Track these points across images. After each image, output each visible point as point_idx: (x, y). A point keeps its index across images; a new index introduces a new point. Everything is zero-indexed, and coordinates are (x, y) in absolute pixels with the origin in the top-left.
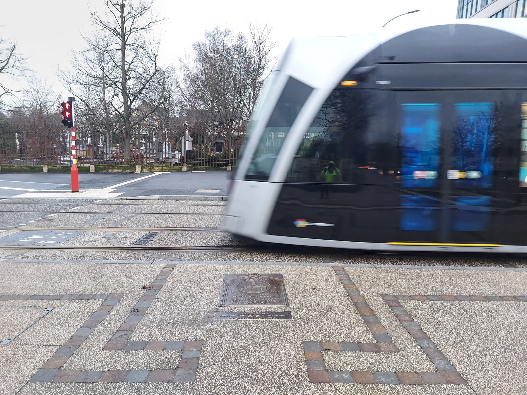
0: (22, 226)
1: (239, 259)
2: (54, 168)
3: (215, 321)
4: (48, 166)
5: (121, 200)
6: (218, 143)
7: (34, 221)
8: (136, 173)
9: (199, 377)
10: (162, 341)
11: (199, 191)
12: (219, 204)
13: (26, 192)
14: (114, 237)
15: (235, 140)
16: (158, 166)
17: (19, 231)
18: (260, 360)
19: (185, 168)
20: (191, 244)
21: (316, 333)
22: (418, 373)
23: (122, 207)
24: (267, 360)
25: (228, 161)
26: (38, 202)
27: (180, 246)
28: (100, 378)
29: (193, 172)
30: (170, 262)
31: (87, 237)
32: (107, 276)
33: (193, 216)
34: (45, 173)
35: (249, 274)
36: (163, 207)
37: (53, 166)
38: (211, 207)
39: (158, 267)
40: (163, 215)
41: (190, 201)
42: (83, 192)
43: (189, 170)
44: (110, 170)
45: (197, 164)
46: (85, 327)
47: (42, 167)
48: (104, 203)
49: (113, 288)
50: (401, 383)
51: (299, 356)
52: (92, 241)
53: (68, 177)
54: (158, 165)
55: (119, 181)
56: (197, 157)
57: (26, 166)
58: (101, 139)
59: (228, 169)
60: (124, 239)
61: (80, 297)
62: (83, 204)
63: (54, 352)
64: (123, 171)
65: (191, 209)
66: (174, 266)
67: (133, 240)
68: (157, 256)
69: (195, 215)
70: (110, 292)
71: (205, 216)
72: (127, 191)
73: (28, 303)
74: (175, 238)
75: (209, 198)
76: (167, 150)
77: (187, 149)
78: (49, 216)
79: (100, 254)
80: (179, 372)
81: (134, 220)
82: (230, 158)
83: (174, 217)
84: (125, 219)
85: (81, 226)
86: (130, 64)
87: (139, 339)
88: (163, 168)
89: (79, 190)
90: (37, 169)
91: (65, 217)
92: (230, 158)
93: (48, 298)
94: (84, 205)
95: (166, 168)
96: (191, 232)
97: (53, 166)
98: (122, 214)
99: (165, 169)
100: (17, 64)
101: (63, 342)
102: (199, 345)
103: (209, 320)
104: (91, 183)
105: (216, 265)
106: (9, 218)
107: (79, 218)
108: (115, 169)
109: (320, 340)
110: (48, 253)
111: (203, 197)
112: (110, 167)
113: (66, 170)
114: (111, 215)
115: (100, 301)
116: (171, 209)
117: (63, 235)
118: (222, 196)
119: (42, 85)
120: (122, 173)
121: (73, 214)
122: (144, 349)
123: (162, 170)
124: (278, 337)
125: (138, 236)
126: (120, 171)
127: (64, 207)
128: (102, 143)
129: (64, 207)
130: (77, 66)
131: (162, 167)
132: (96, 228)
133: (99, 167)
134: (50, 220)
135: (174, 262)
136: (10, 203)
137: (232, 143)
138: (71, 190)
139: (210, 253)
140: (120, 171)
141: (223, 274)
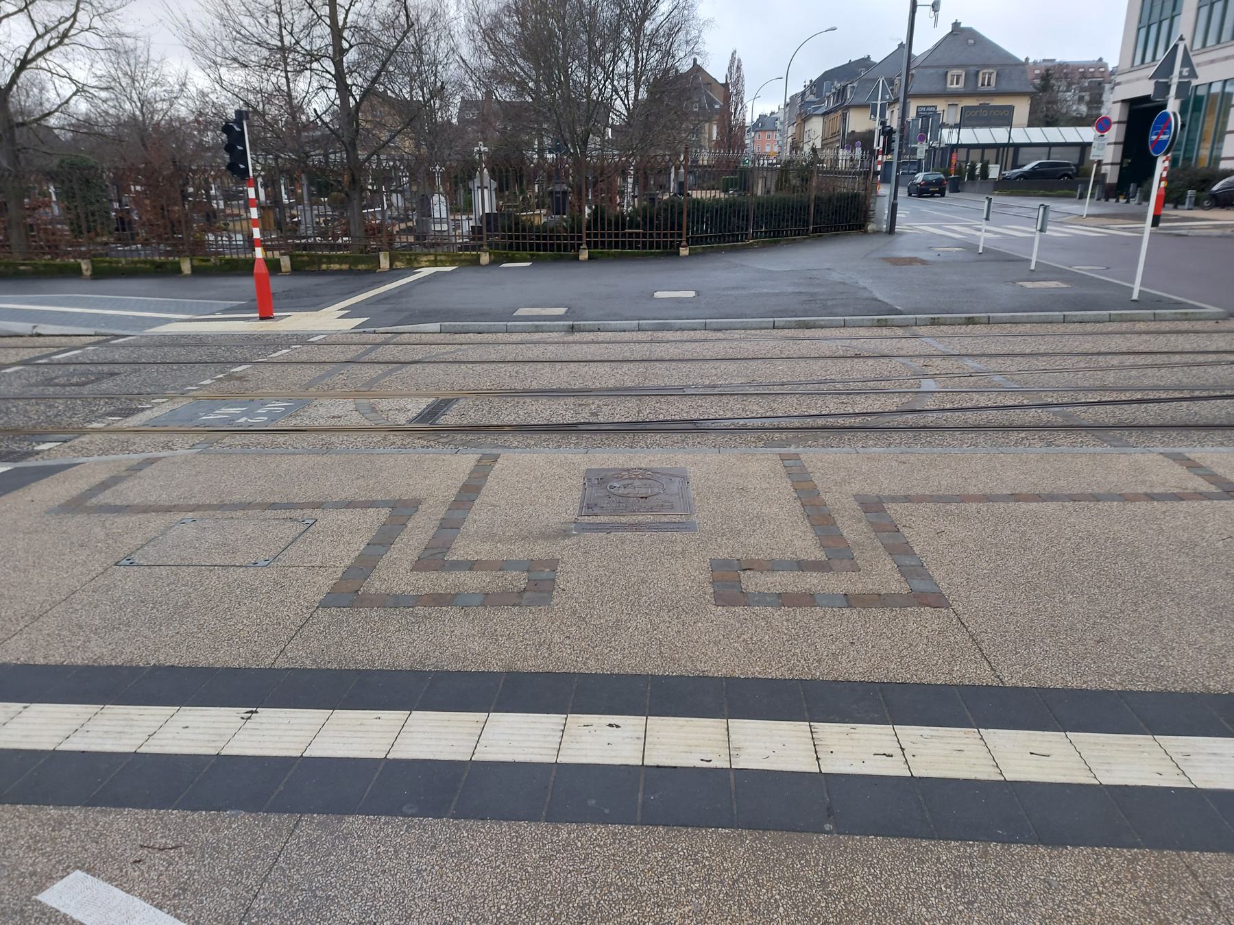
0: (193, 390)
1: (609, 445)
2: (203, 264)
3: (574, 535)
4: (191, 260)
5: (364, 335)
6: (557, 193)
7: (211, 382)
8: (380, 272)
9: (555, 601)
10: (496, 561)
11: (522, 312)
12: (566, 339)
13: (169, 321)
14: (374, 410)
15: (595, 184)
16: (426, 255)
17: (191, 400)
18: (644, 582)
19: (485, 258)
20: (519, 421)
21: (733, 549)
22: (880, 595)
23: (371, 351)
24: (655, 581)
25: (580, 238)
26: (199, 341)
27: (500, 424)
28: (417, 602)
29: (504, 265)
30: (488, 451)
31: (322, 411)
32: (385, 474)
33: (516, 367)
34: (186, 276)
35: (628, 470)
36: (453, 348)
37: (203, 260)
38: (551, 348)
39: (466, 461)
40: (457, 366)
41: (505, 334)
42: (282, 318)
43: (495, 262)
44: (324, 267)
45: (511, 247)
46: (374, 544)
47: (178, 263)
48: (331, 341)
49: (402, 489)
50: (849, 606)
51: (704, 576)
52: (334, 417)
53: (247, 285)
54: (425, 250)
55: (350, 293)
56: (510, 230)
57: (145, 262)
58: (283, 187)
59: (581, 257)
60: (394, 412)
61: (350, 505)
62: (291, 345)
63: (340, 575)
64: (353, 267)
65: (510, 352)
66: (496, 458)
67: (409, 413)
68: (461, 442)
69: (520, 364)
70: (398, 497)
71: (540, 366)
72: (376, 312)
73: (280, 513)
74: (487, 409)
75: (544, 328)
76: (444, 215)
77: (487, 211)
78: (234, 370)
79: (356, 439)
80: (527, 595)
81: (402, 376)
82: (585, 231)
83: (478, 368)
84: (385, 375)
85: (302, 390)
86: (347, 11)
87: (460, 559)
88: (439, 258)
89: (275, 314)
90: (169, 266)
91: (268, 372)
92: (585, 231)
93: (301, 506)
94: (293, 347)
95: (443, 258)
96: (516, 399)
97: (203, 260)
98: (376, 365)
99: (441, 261)
100: (97, 23)
101: (348, 562)
102: (553, 564)
103: (565, 534)
104: (292, 298)
105: (570, 456)
106: (160, 376)
107: (295, 375)
108: (334, 263)
109: (739, 556)
110: (264, 438)
111: (532, 325)
112: (324, 260)
113: (243, 268)
114: (353, 365)
115: (387, 510)
116: (471, 353)
117: (277, 406)
118: (571, 323)
119: (141, 60)
120: (350, 272)
121: (279, 365)
122: (470, 569)
123: (435, 263)
124: (673, 555)
125: (417, 406)
126: (345, 267)
127: (255, 351)
128: (286, 197)
129: (255, 351)
130: (231, 23)
131: (436, 256)
132: (333, 391)
133: (299, 259)
134: (240, 379)
135: (495, 451)
136: (148, 346)
137: (587, 191)
138: (257, 315)
139: (556, 437)
140: (345, 267)
141: (584, 468)
